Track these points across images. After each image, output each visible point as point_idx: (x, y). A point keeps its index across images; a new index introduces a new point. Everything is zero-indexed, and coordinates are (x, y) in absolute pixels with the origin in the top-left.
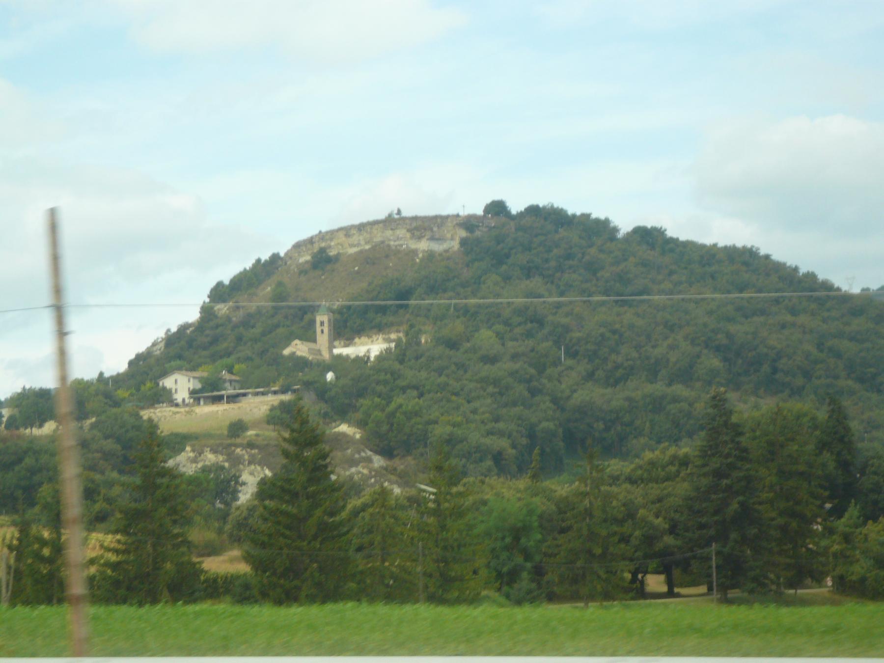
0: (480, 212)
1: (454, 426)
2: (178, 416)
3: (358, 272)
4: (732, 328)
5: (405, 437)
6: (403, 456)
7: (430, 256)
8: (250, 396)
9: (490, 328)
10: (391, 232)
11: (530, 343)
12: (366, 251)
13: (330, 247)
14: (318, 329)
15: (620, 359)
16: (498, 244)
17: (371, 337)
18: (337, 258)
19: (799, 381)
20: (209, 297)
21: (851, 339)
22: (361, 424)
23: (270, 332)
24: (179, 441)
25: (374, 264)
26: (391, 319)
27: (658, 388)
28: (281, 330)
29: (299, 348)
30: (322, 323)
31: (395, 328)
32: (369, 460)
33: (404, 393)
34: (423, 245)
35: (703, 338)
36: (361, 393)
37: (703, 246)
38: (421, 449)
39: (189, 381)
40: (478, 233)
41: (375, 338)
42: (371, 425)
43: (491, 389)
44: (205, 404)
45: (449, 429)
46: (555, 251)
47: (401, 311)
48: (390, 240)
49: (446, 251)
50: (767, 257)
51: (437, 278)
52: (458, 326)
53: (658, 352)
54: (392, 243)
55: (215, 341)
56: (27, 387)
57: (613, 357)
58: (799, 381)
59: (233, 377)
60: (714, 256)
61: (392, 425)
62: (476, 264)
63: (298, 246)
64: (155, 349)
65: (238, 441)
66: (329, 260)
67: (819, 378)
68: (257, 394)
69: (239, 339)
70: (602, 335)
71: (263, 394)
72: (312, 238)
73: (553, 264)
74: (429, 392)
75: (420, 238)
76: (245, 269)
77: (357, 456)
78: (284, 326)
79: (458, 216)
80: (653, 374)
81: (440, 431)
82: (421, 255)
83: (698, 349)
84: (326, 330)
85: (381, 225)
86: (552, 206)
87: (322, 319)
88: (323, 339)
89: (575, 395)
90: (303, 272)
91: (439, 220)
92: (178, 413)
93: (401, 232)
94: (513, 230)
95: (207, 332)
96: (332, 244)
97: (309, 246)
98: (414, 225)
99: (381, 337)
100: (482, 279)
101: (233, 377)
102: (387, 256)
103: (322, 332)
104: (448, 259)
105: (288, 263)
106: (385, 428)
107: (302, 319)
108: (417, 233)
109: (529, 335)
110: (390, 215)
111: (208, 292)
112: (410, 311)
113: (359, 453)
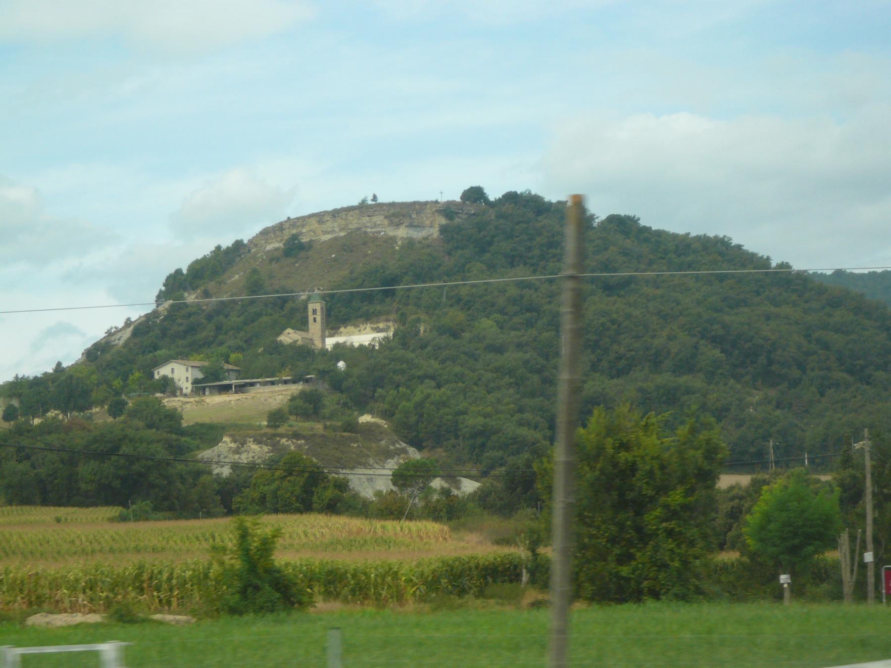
0: (458, 199)
1: (485, 416)
2: (188, 406)
3: (335, 260)
4: (727, 319)
5: (436, 429)
6: (433, 448)
7: (410, 244)
8: (258, 385)
9: (487, 317)
10: (367, 218)
11: (534, 332)
12: (342, 237)
13: (301, 233)
14: (311, 318)
15: (622, 350)
16: (480, 232)
17: (358, 326)
18: (308, 247)
19: (796, 373)
20: (164, 285)
21: (837, 331)
22: (387, 414)
23: (253, 321)
24: (209, 433)
25: (352, 251)
26: (378, 307)
27: (664, 379)
28: (264, 319)
29: (289, 337)
30: (314, 312)
31: (383, 317)
32: (405, 451)
33: (422, 383)
34: (402, 232)
35: (699, 329)
36: (379, 383)
37: (675, 236)
38: (453, 441)
39: (187, 370)
40: (457, 220)
41: (362, 327)
42: (397, 416)
43: (507, 379)
44: (211, 393)
45: (481, 420)
46: (538, 239)
47: (388, 300)
48: (367, 227)
49: (425, 239)
50: (739, 247)
51: (420, 266)
52: (456, 315)
53: (656, 342)
54: (369, 230)
55: (192, 329)
56: (20, 376)
57: (615, 347)
58: (796, 373)
59: (230, 367)
60: (688, 246)
61: (421, 416)
62: (459, 252)
63: (265, 233)
64: (113, 338)
65: (281, 430)
66: (302, 247)
67: (813, 370)
68: (265, 384)
69: (219, 328)
70: (603, 324)
71: (273, 383)
72: (281, 224)
73: (537, 252)
74: (447, 382)
75: (398, 225)
76: (688, 234)
77: (392, 447)
78: (266, 315)
79: (436, 202)
80: (656, 362)
81: (473, 421)
82: (400, 243)
83: (695, 339)
84: (319, 318)
85: (357, 211)
86: (530, 193)
87: (316, 307)
88: (315, 328)
89: (586, 386)
90: (273, 258)
91: (417, 207)
92: (187, 402)
93: (379, 219)
94: (493, 217)
95: (179, 321)
96: (304, 231)
97: (278, 233)
98: (392, 211)
99: (368, 326)
100: (467, 267)
101: (230, 367)
102: (365, 244)
103: (315, 320)
104: (428, 246)
105: (253, 251)
106: (413, 419)
107: (282, 308)
108: (396, 220)
109: (529, 324)
110: (364, 201)
111: (164, 281)
112: (397, 300)
113: (394, 445)
